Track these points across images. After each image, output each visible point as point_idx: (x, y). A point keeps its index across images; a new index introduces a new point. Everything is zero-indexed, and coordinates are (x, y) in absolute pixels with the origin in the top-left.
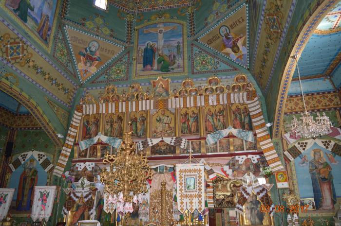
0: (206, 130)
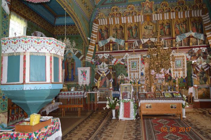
0: (175, 33)
